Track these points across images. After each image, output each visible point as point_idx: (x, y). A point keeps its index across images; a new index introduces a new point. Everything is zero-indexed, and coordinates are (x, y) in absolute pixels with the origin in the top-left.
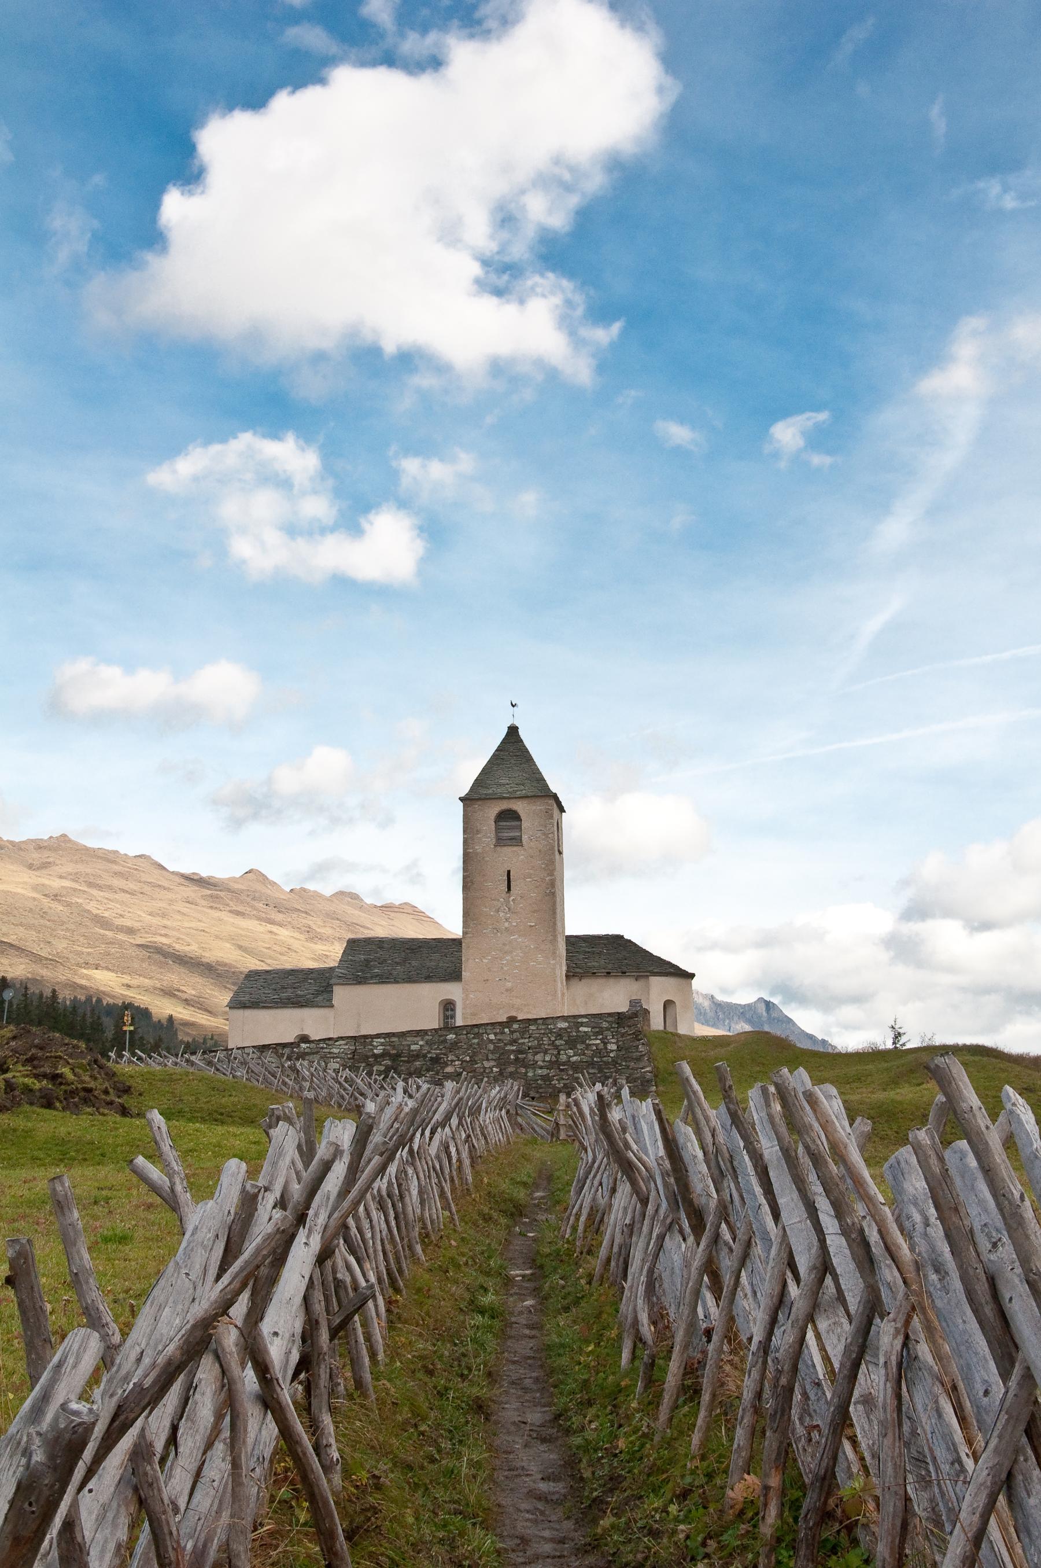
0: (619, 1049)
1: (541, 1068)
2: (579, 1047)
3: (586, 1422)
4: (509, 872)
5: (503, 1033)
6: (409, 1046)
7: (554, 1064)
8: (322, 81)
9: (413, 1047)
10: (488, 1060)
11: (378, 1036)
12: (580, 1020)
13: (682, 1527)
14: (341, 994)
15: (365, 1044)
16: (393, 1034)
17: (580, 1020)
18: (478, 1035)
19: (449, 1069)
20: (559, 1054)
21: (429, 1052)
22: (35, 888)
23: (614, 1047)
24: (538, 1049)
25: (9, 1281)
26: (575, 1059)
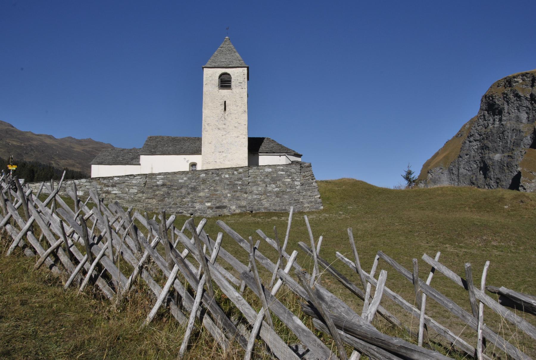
2: (278, 183)
4: (225, 102)
5: (233, 174)
6: (178, 180)
7: (265, 193)
9: (180, 181)
10: (224, 189)
11: (160, 174)
12: (278, 168)
14: (143, 159)
15: (151, 178)
16: (169, 173)
19: (201, 194)
20: (266, 186)
21: (190, 184)
22: (83, 150)
23: (299, 183)
24: (256, 184)
26: (276, 189)
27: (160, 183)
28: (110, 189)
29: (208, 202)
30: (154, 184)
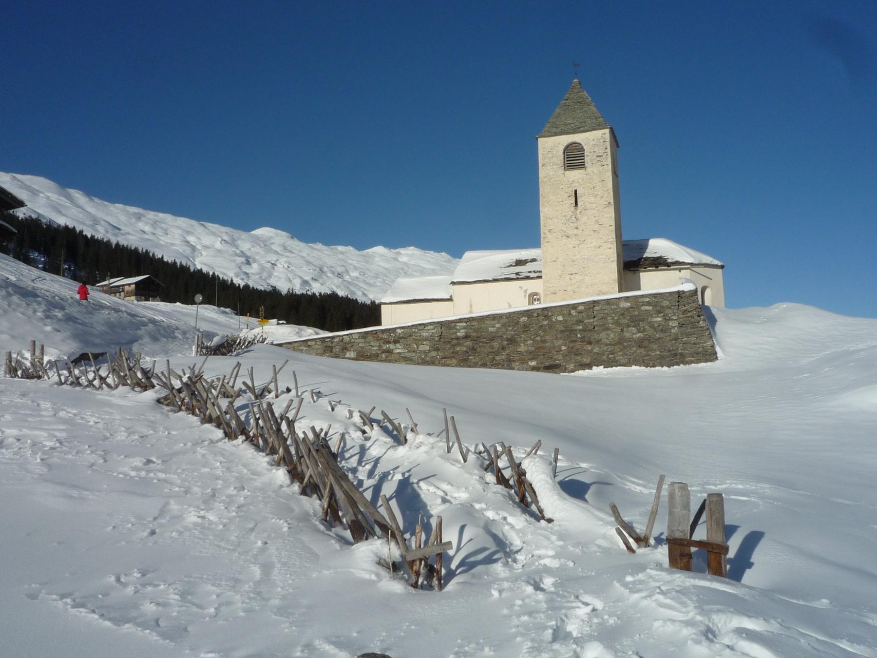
0: (681, 326)
1: (607, 345)
3: (727, 641)
4: (576, 191)
8: (750, 565)
12: (641, 300)
13: (234, 514)
17: (641, 300)
18: (546, 317)
21: (504, 334)
25: (720, 655)
27: (461, 334)
28: (392, 346)
29: (532, 359)
30: (453, 336)
